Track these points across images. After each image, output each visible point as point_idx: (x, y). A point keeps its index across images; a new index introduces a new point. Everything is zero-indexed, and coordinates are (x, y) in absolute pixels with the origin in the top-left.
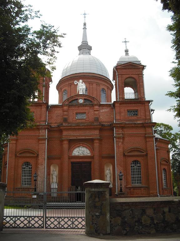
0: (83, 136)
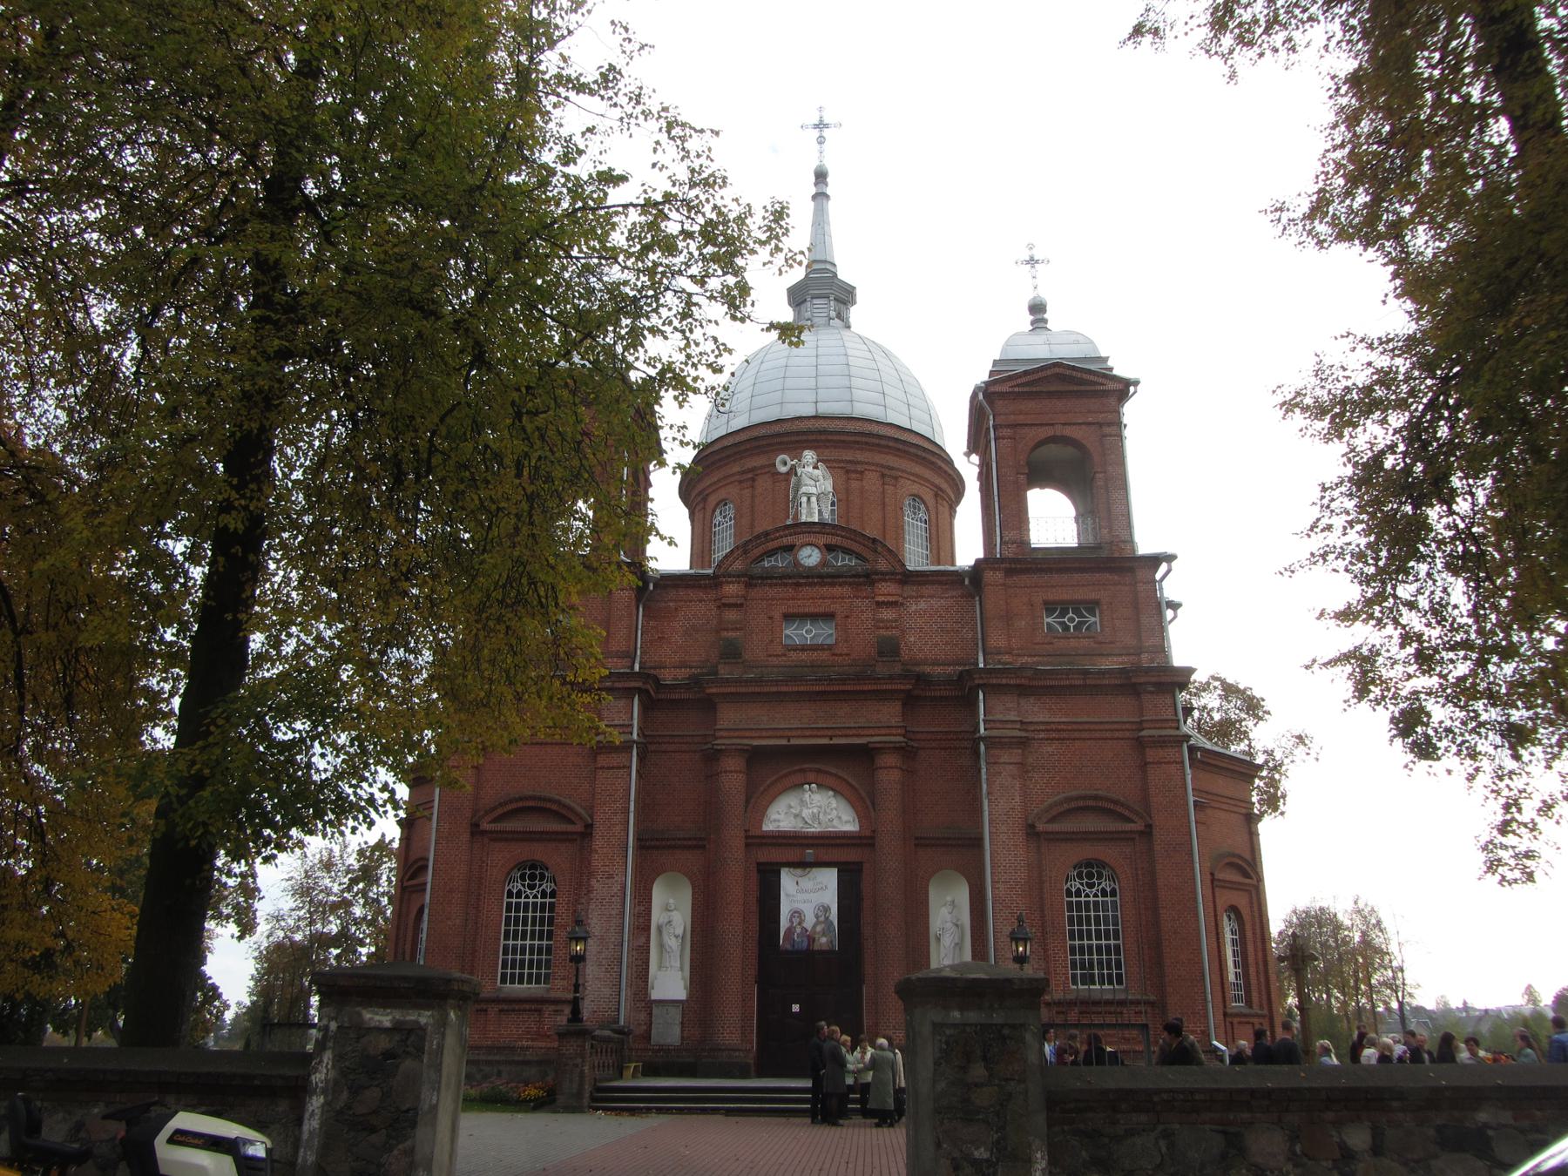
0: (821, 733)
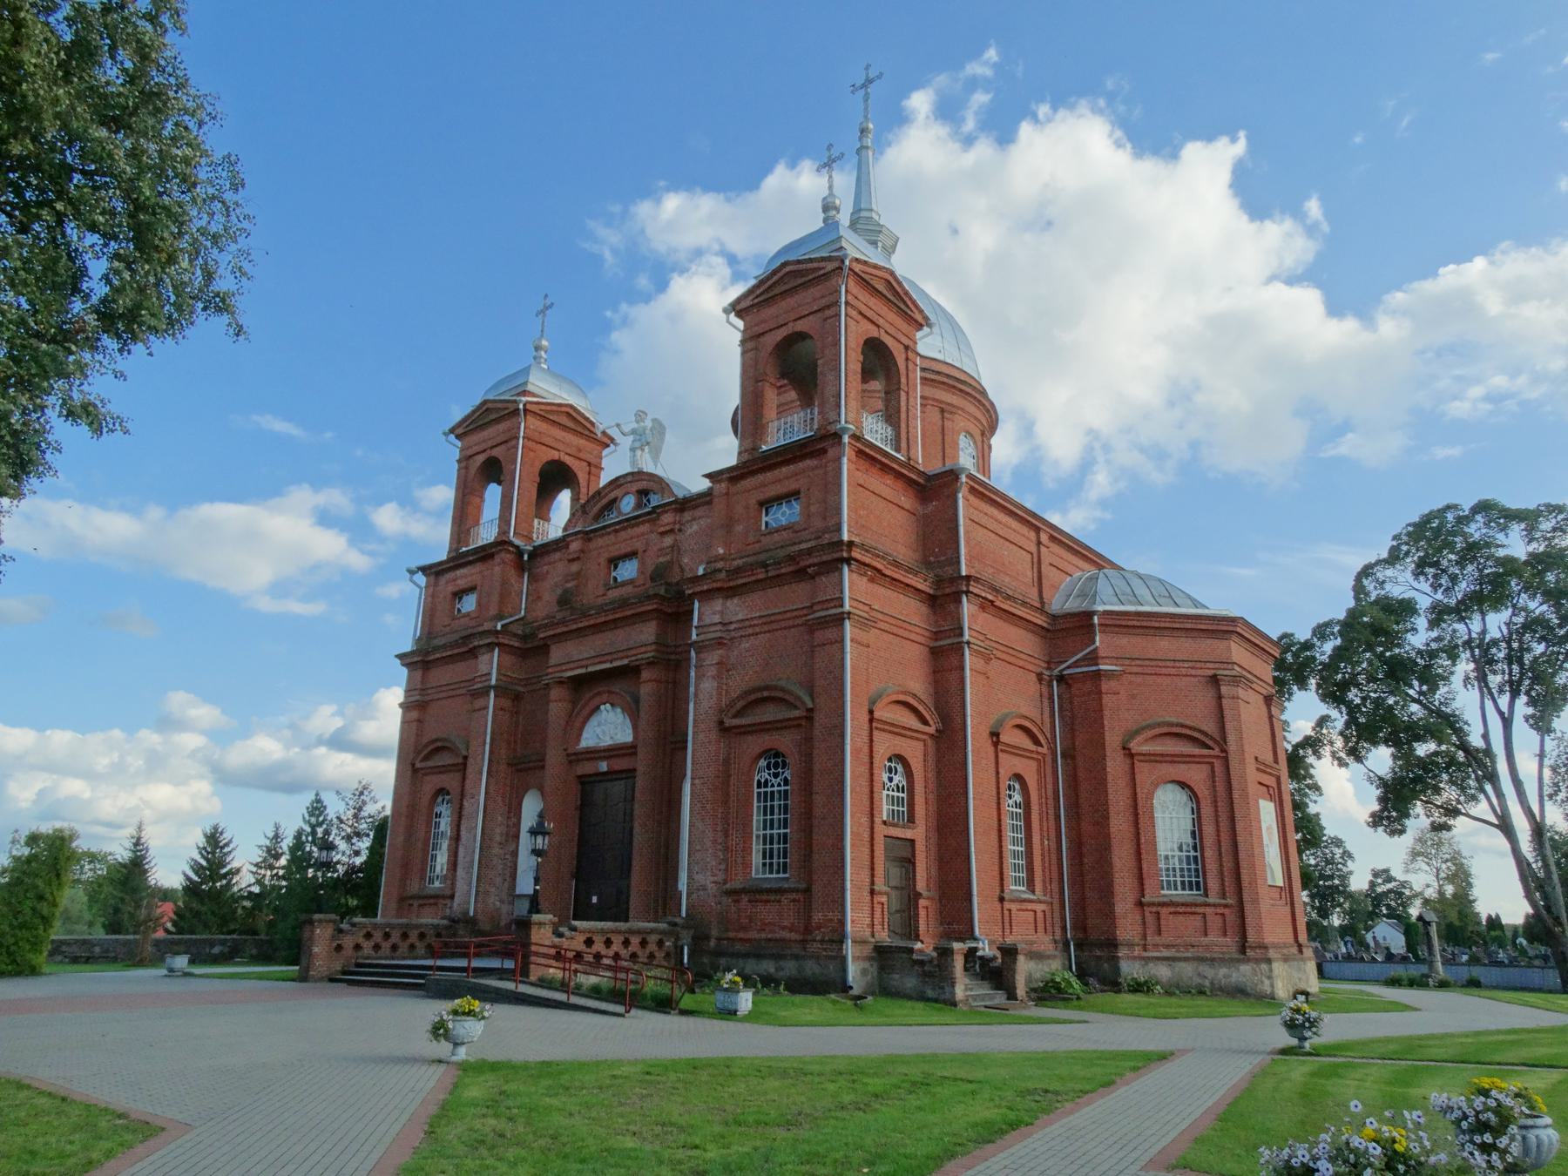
0: (606, 658)
